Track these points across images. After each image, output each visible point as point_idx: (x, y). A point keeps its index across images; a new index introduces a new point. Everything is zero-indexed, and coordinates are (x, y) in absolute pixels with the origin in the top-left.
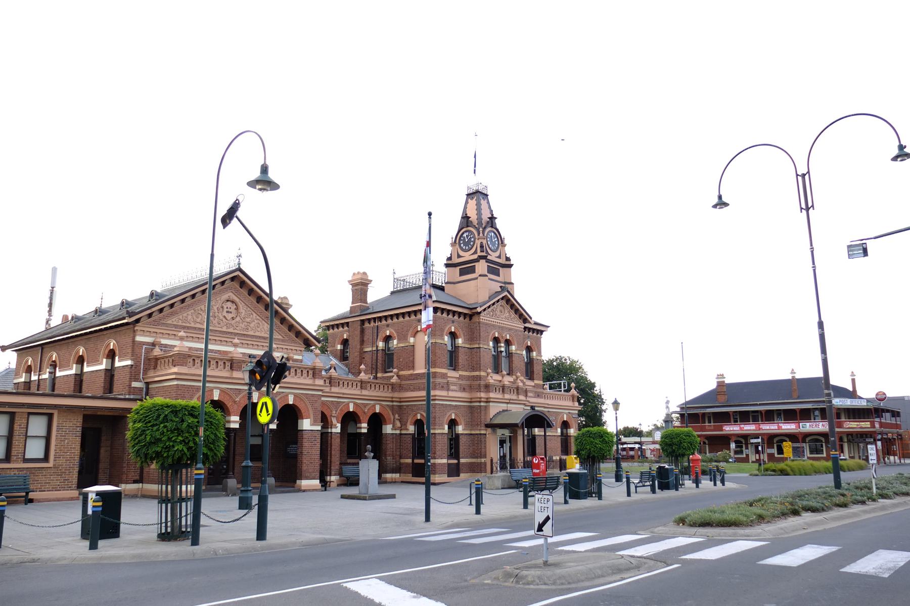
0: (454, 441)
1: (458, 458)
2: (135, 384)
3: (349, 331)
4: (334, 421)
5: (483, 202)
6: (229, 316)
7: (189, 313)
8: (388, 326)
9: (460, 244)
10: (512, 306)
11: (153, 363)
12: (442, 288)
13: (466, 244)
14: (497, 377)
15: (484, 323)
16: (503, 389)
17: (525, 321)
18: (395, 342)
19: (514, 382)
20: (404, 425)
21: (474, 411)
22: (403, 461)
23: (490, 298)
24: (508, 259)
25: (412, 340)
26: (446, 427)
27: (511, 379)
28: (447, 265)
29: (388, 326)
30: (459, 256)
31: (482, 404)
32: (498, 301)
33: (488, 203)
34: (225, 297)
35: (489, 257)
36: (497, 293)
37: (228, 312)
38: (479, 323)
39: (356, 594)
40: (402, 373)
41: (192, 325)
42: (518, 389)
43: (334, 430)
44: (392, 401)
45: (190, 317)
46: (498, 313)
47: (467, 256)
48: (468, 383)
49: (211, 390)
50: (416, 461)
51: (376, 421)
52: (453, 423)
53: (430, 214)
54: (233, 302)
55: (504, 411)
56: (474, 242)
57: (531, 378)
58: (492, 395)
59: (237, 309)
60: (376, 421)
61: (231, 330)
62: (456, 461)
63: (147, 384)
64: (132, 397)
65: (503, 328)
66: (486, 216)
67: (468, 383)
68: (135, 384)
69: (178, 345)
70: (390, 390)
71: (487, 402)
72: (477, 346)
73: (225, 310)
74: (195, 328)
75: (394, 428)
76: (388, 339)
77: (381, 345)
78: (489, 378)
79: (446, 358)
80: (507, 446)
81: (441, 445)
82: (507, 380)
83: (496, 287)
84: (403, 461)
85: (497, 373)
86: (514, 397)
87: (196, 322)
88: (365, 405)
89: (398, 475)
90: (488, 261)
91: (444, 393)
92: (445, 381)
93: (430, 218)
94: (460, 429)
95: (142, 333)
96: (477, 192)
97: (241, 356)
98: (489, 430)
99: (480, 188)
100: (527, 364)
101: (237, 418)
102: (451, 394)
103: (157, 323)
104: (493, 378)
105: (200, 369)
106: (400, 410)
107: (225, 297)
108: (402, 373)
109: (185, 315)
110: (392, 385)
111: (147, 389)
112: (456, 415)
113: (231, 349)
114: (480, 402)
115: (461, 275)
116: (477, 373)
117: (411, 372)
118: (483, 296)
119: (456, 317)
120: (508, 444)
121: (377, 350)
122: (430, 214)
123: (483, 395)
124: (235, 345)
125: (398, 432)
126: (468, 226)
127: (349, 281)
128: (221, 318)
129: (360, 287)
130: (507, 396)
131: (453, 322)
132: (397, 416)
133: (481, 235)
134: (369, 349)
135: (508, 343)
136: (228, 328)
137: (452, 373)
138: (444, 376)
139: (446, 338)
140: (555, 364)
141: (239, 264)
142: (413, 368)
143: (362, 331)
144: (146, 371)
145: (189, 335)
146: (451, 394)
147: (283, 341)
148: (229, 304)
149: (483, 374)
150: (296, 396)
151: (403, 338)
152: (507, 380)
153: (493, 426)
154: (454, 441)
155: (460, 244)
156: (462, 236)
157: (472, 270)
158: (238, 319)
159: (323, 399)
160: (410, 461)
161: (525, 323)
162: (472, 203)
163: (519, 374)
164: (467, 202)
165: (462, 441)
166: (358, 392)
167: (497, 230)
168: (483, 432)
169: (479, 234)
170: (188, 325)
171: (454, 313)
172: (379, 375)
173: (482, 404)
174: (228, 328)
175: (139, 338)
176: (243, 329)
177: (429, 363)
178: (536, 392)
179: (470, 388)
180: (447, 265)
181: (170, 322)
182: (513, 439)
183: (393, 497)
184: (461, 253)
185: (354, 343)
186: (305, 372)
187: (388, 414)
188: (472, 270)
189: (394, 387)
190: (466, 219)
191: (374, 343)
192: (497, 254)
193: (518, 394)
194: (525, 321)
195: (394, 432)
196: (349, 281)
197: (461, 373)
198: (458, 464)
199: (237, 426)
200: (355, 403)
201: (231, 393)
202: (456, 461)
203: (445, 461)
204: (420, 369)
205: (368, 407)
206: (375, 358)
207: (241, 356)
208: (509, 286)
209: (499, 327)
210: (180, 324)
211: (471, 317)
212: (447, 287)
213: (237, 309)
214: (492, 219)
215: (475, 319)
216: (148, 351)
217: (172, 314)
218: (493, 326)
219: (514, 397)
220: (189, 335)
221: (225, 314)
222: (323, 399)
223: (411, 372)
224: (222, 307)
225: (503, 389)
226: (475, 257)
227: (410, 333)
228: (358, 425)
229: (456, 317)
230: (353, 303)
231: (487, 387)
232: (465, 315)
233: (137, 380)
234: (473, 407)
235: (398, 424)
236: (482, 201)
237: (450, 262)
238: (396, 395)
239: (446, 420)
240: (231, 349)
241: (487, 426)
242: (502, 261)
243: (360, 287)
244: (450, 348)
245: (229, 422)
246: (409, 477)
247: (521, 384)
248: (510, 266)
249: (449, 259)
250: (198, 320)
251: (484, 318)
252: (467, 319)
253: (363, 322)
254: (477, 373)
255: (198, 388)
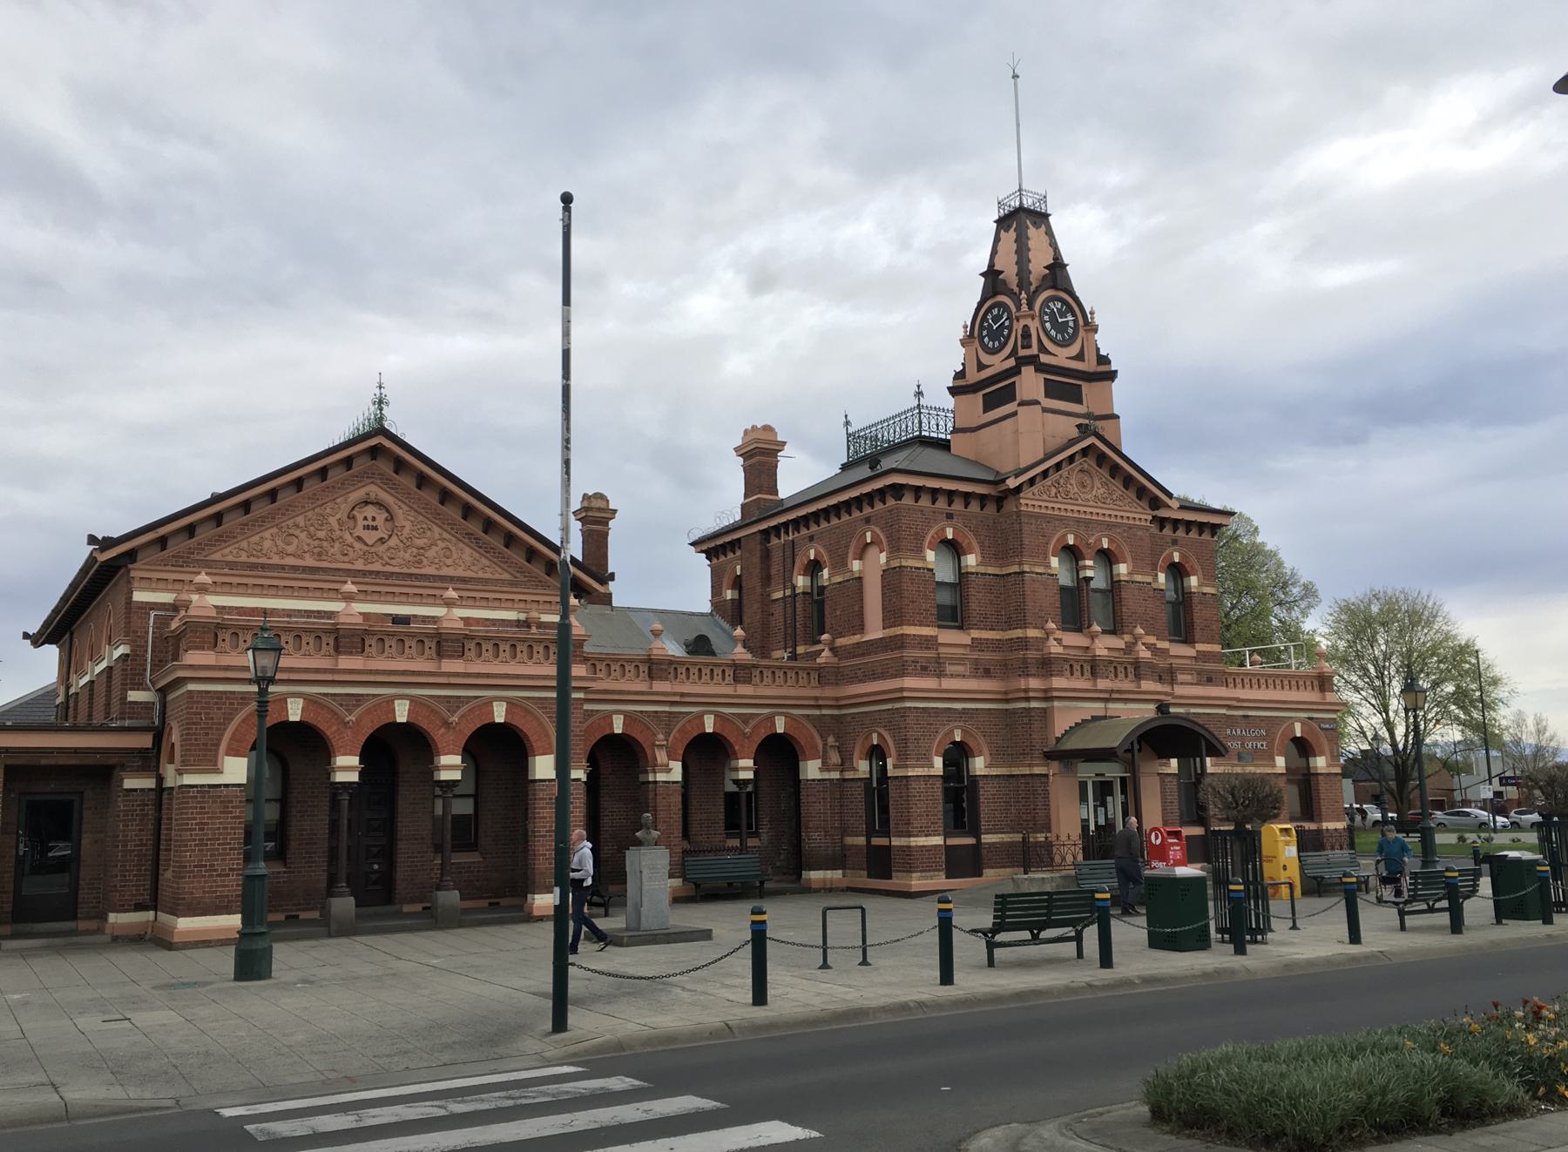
0: (960, 798)
1: (976, 832)
2: (135, 696)
3: (741, 558)
4: (661, 756)
5: (1035, 235)
6: (371, 537)
7: (267, 534)
8: (868, 520)
9: (981, 338)
10: (1115, 470)
11: (171, 645)
12: (944, 445)
13: (994, 335)
14: (1074, 639)
15: (1030, 515)
16: (1094, 667)
17: (1155, 503)
18: (826, 573)
19: (1130, 648)
20: (846, 763)
21: (1016, 728)
22: (850, 840)
23: (1048, 457)
24: (1104, 360)
25: (856, 565)
26: (938, 762)
27: (1118, 642)
28: (954, 391)
29: (811, 538)
30: (981, 367)
31: (1034, 704)
32: (1071, 459)
33: (1049, 233)
34: (357, 495)
35: (1044, 358)
36: (1072, 442)
37: (367, 527)
38: (1019, 513)
39: (793, 1122)
40: (840, 642)
41: (276, 560)
42: (1137, 664)
43: (661, 777)
44: (819, 707)
45: (267, 544)
46: (1074, 489)
47: (998, 363)
48: (996, 656)
49: (283, 700)
50: (951, 842)
51: (780, 753)
52: (957, 755)
53: (567, 199)
54: (379, 504)
55: (1095, 718)
56: (1010, 328)
57: (1188, 640)
58: (1058, 682)
59: (391, 518)
60: (780, 753)
61: (377, 567)
62: (970, 841)
63: (163, 692)
64: (127, 723)
65: (1087, 523)
66: (1039, 262)
67: (996, 656)
68: (135, 696)
69: (207, 603)
70: (814, 683)
71: (1046, 699)
72: (1015, 569)
73: (361, 523)
74: (283, 567)
75: (825, 767)
76: (814, 568)
77: (801, 582)
78: (1052, 642)
79: (1164, 617)
80: (1115, 803)
81: (929, 804)
82: (1104, 646)
83: (1066, 428)
84: (850, 840)
85: (1079, 630)
86: (1127, 685)
87: (283, 554)
88: (745, 719)
89: (838, 874)
90: (1041, 368)
91: (929, 683)
92: (931, 654)
93: (567, 209)
94: (979, 765)
95: (144, 584)
96: (1021, 210)
97: (461, 625)
98: (1053, 768)
99: (1028, 202)
100: (1175, 605)
101: (354, 761)
102: (947, 683)
103: (183, 561)
104: (1061, 643)
105: (409, 653)
106: (839, 729)
107: (357, 495)
108: (840, 642)
109: (256, 539)
110: (819, 669)
111: (164, 705)
112: (964, 732)
113: (439, 611)
114: (1028, 699)
115: (985, 412)
116: (1019, 633)
117: (856, 638)
118: (1030, 450)
119: (1181, 533)
120: (1119, 798)
121: (794, 595)
122: (567, 199)
123: (1034, 683)
124: (449, 604)
125: (835, 775)
126: (995, 294)
127: (736, 449)
128: (350, 540)
129: (760, 457)
130: (1102, 684)
131: (950, 516)
132: (831, 740)
133: (1025, 307)
134: (778, 595)
135: (1107, 558)
136: (367, 562)
137: (948, 636)
138: (929, 643)
139: (1162, 577)
140: (1375, 609)
141: (381, 418)
142: (861, 628)
143: (766, 555)
144: (158, 664)
145: (219, 579)
146: (947, 683)
147: (512, 584)
148: (370, 511)
149: (1032, 633)
150: (511, 703)
151: (840, 563)
152: (1104, 646)
153: (1066, 757)
154: (960, 798)
155: (981, 338)
156: (984, 318)
157: (1008, 395)
158: (393, 542)
159: (587, 707)
160: (862, 840)
161: (1157, 508)
162: (1009, 237)
163: (1140, 631)
164: (997, 240)
165: (986, 794)
166: (729, 690)
167: (1076, 300)
168: (1037, 770)
169: (1019, 308)
170: (263, 560)
171: (951, 495)
172: (800, 650)
173: (1034, 704)
174: (367, 562)
175: (139, 596)
176: (408, 564)
177: (893, 616)
178: (1199, 673)
179: (1005, 670)
180: (954, 391)
181: (217, 556)
182: (1131, 788)
183: (706, 935)
184: (986, 359)
185: (753, 583)
186: (1077, 667)
187: (808, 736)
188: (1008, 395)
189: (824, 676)
190: (992, 275)
191: (788, 581)
192: (1074, 350)
193: (1094, 674)
194: (1155, 503)
195: (826, 776)
196: (736, 449)
197: (975, 634)
198: (978, 846)
199: (354, 777)
200: (717, 715)
201: (334, 705)
202: (970, 841)
203: (937, 840)
204: (875, 631)
205: (752, 723)
206: (789, 610)
207: (461, 625)
208: (1104, 427)
209: (1078, 521)
210: (244, 558)
211: (1000, 500)
212: (959, 445)
213: (391, 518)
214: (1057, 268)
215: (1009, 506)
216: (162, 623)
217: (221, 539)
218: (1061, 519)
219: (1127, 685)
220: (219, 579)
221: (359, 531)
222: (587, 707)
223: (856, 638)
224: (352, 517)
225: (1094, 667)
226: (1012, 362)
227: (851, 555)
228: (733, 763)
229: (1181, 533)
230: (746, 496)
231: (1047, 666)
232: (983, 499)
233: (139, 686)
234: (1014, 711)
235: (835, 758)
236: (1032, 232)
237: (961, 383)
238: (829, 692)
239: (938, 741)
240: (439, 611)
241: (1050, 756)
242: (1089, 365)
243: (760, 457)
244: (1171, 595)
245: (737, 769)
246: (862, 879)
247: (1144, 654)
248: (1111, 376)
249: (960, 375)
250: (290, 549)
251: (1029, 502)
252: (991, 509)
253: (766, 533)
254: (1019, 633)
255: (244, 697)
